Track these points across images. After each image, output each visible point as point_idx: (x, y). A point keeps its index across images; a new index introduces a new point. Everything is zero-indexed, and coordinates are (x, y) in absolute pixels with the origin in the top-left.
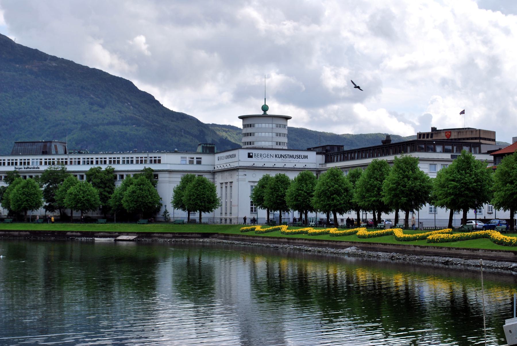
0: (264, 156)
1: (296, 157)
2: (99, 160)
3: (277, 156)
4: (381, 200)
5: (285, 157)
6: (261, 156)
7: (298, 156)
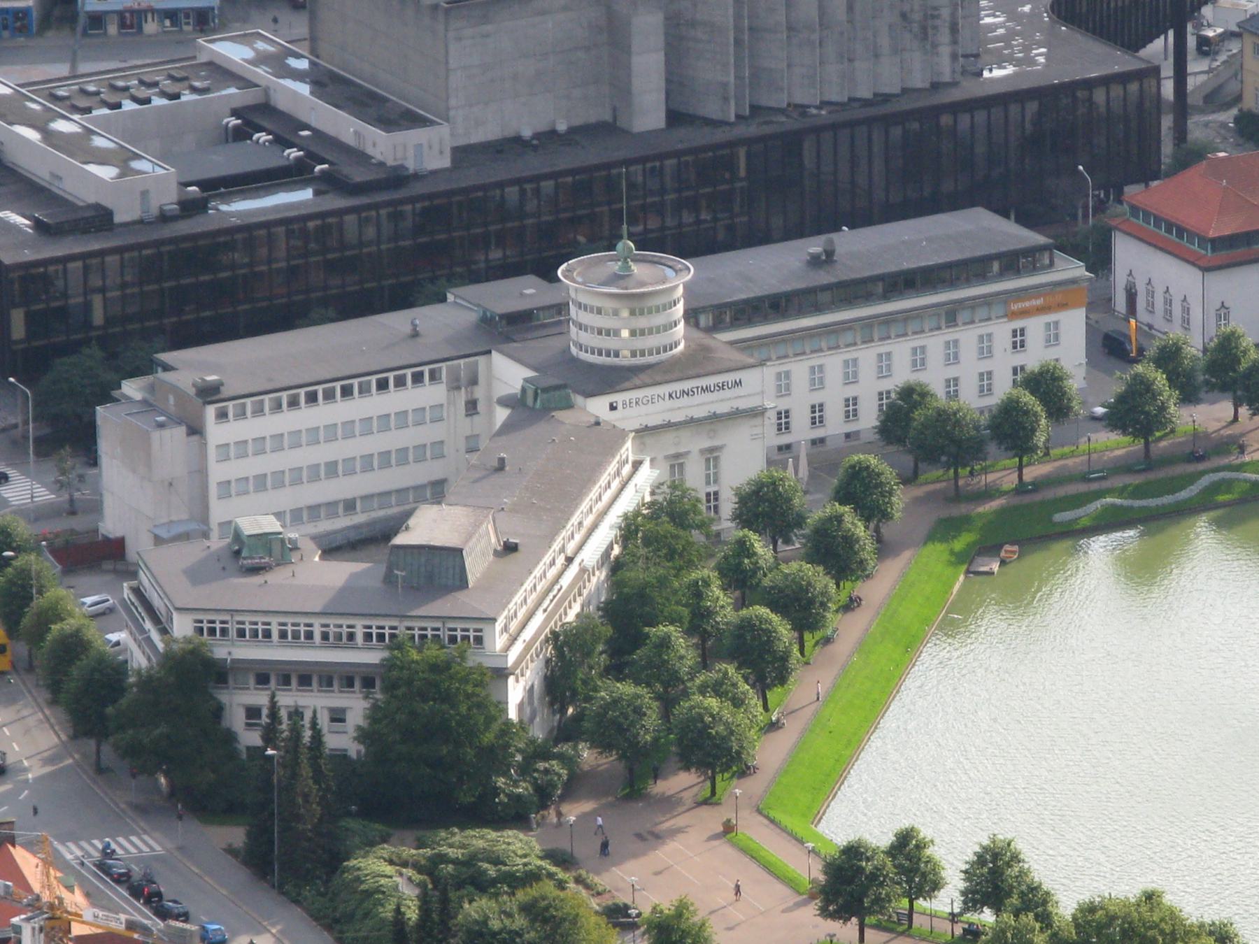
0: (645, 402)
1: (717, 388)
2: (289, 629)
3: (674, 395)
4: (601, 617)
5: (691, 393)
6: (636, 402)
7: (720, 385)
